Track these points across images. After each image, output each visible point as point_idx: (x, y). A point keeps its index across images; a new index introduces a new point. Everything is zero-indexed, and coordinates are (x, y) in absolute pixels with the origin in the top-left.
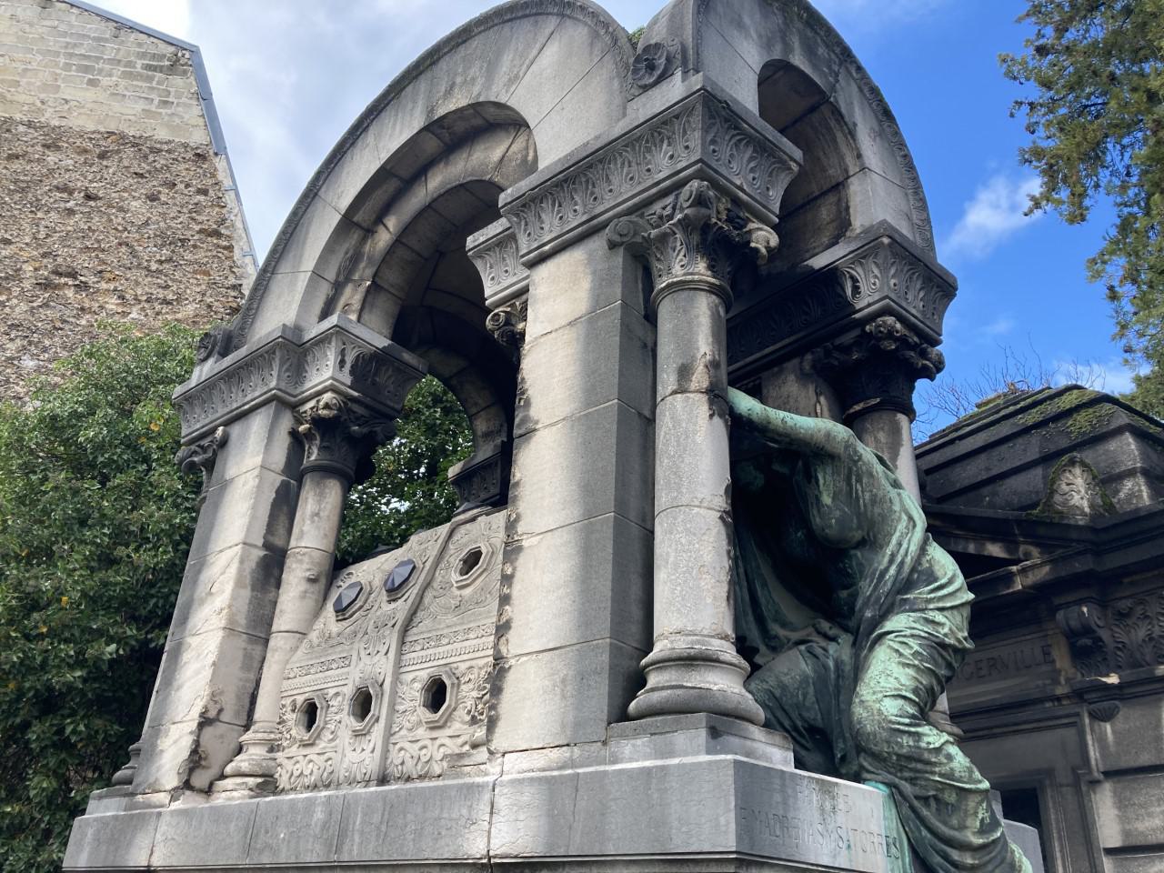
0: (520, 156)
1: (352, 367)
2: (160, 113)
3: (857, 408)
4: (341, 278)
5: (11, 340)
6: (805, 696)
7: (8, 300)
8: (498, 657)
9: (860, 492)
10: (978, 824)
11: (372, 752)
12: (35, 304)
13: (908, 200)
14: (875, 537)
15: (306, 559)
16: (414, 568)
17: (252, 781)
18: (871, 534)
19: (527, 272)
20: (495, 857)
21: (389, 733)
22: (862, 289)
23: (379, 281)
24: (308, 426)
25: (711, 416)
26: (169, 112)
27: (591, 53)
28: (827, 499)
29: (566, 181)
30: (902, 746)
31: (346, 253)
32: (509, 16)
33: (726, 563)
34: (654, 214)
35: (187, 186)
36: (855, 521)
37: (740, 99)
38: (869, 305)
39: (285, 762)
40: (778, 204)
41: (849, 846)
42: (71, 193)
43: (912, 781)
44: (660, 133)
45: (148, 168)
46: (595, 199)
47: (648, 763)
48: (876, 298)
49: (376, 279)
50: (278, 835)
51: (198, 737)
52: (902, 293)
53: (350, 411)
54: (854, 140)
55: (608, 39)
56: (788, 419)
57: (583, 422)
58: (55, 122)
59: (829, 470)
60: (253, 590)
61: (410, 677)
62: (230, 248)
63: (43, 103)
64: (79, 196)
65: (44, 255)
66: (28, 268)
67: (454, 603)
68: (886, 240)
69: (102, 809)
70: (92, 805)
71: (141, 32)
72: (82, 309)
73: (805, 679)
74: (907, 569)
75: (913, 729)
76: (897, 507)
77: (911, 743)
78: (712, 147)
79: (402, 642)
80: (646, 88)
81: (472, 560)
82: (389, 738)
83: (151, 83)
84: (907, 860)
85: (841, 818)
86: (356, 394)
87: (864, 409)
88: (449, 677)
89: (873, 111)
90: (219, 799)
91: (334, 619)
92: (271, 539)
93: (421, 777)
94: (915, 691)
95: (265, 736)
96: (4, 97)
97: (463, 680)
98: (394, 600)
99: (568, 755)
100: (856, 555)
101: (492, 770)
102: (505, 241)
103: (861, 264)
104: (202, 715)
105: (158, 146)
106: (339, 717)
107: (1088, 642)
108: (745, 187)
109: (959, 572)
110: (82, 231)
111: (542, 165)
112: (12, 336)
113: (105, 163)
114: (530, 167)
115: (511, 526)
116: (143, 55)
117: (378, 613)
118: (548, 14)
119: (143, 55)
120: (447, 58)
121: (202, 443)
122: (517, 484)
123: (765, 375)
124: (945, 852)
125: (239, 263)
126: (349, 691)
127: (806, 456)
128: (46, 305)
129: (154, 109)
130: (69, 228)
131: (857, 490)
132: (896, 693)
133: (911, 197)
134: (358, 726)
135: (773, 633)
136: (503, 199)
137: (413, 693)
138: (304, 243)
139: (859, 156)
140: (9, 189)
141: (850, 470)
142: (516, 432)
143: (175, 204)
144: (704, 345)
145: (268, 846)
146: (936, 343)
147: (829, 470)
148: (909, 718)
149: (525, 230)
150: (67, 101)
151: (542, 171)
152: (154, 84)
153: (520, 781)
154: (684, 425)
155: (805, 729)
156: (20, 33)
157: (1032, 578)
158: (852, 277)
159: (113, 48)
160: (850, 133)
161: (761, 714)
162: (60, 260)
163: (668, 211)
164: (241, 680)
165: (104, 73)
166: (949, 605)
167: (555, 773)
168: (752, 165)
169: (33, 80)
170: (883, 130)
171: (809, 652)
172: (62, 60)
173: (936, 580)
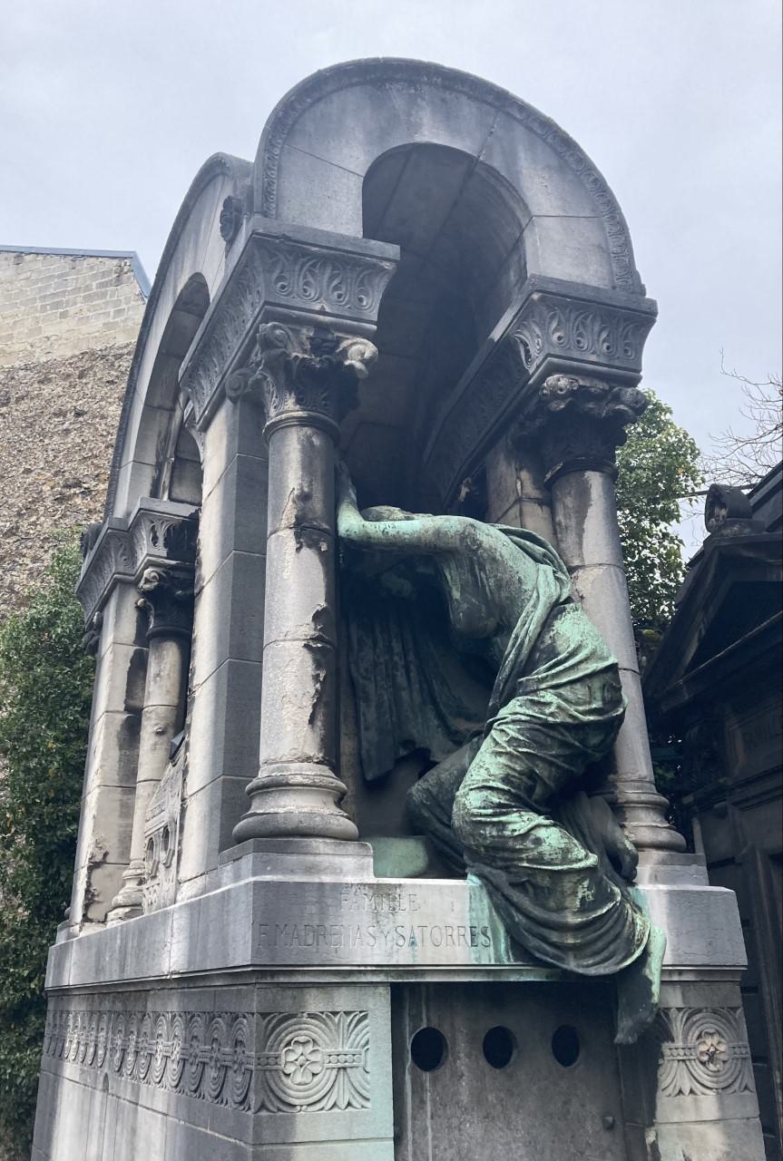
1: (165, 540)
2: (117, 322)
5: (46, 551)
7: (38, 519)
9: (484, 580)
10: (578, 903)
12: (56, 517)
13: (604, 229)
15: (153, 716)
18: (503, 618)
23: (182, 455)
25: (298, 550)
26: (123, 318)
28: (456, 594)
30: (485, 838)
31: (159, 436)
36: (483, 610)
38: (538, 367)
42: (65, 416)
43: (506, 869)
45: (115, 374)
49: (178, 454)
53: (173, 578)
58: (43, 359)
59: (453, 565)
60: (120, 749)
63: (32, 346)
64: (70, 416)
65: (56, 474)
66: (46, 488)
71: (92, 257)
72: (90, 511)
74: (525, 651)
75: (495, 819)
77: (494, 833)
83: (105, 298)
84: (503, 946)
85: (401, 918)
86: (173, 562)
89: (551, 146)
90: (110, 925)
92: (132, 702)
94: (506, 780)
96: (4, 351)
100: (497, 642)
105: (121, 351)
108: (328, 310)
110: (78, 445)
112: (46, 548)
113: (84, 381)
116: (94, 277)
119: (94, 277)
124: (541, 935)
127: (425, 560)
128: (64, 516)
129: (112, 321)
130: (69, 445)
131: (481, 579)
133: (606, 224)
135: (453, 728)
140: (22, 427)
146: (634, 381)
147: (453, 565)
148: (491, 808)
150: (48, 338)
152: (108, 298)
156: (6, 293)
158: (522, 341)
159: (73, 279)
161: (351, 827)
162: (67, 474)
164: (121, 826)
165: (70, 304)
168: (335, 283)
169: (21, 330)
170: (566, 162)
172: (39, 304)
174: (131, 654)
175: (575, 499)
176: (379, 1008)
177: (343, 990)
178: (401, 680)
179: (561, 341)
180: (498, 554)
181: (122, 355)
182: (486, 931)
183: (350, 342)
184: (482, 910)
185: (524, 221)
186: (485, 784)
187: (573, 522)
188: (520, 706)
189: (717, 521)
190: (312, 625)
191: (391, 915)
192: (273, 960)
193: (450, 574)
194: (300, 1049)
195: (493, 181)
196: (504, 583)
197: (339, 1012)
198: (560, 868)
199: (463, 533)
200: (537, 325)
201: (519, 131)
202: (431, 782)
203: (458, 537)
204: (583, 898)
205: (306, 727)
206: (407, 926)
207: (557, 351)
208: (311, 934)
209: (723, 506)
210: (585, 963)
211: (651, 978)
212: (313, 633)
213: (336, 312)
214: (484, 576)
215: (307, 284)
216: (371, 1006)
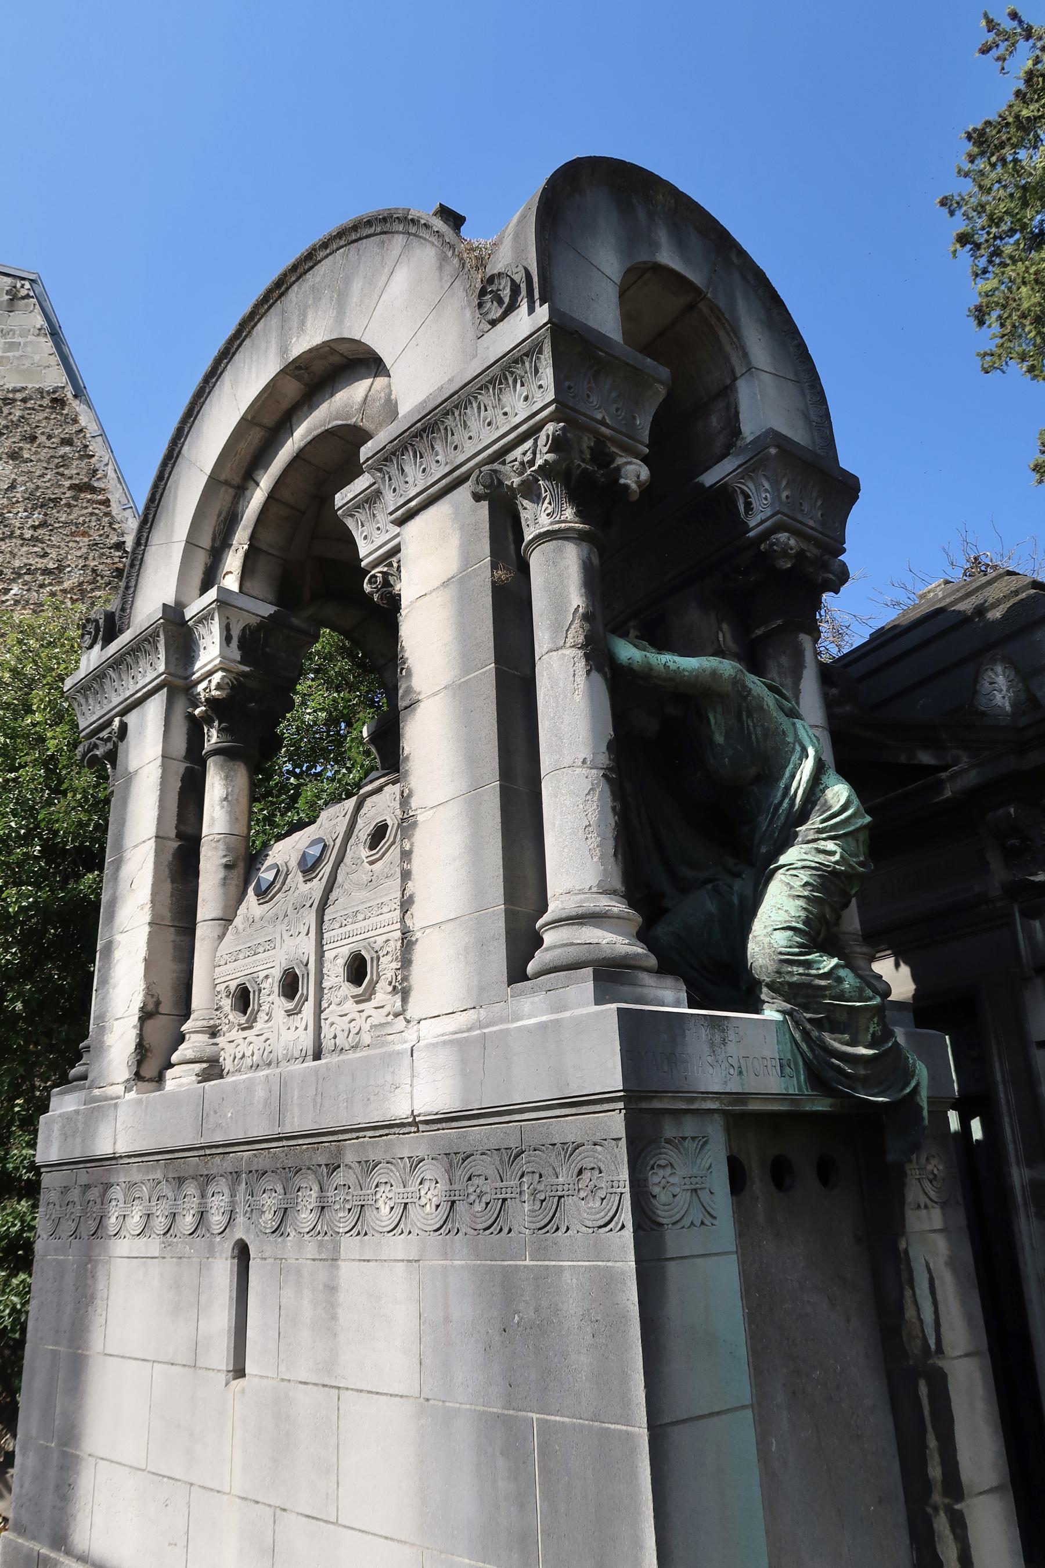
0: (383, 395)
4: (217, 544)
8: (406, 933)
10: (869, 1037)
11: (306, 1029)
16: (325, 846)
17: (198, 1067)
19: (397, 530)
20: (419, 1115)
21: (319, 1011)
22: (754, 505)
24: (203, 708)
25: (588, 672)
26: (17, 354)
27: (441, 279)
28: (719, 739)
29: (424, 430)
31: (219, 516)
32: (354, 237)
34: (516, 460)
35: (49, 437)
37: (592, 323)
38: (762, 522)
39: (227, 1046)
40: (647, 433)
41: (740, 1073)
44: (512, 373)
46: (456, 448)
47: (544, 1018)
48: (769, 514)
50: (226, 1115)
51: (141, 1030)
54: (738, 338)
55: (456, 260)
56: (670, 664)
57: (460, 690)
59: (719, 709)
61: (333, 953)
62: (106, 502)
67: (365, 878)
68: (773, 451)
69: (64, 1104)
70: (52, 1105)
76: (790, 739)
78: (567, 384)
79: (320, 921)
80: (493, 323)
81: (379, 834)
82: (320, 1016)
85: (732, 1048)
86: (247, 669)
87: (764, 633)
88: (368, 951)
90: (170, 1085)
91: (256, 902)
92: (183, 828)
93: (354, 1047)
95: (205, 1023)
97: (381, 953)
98: (309, 880)
99: (476, 1017)
101: (409, 1037)
102: (371, 499)
103: (751, 478)
104: (142, 1009)
105: (11, 396)
106: (271, 1000)
107: (1017, 842)
109: (854, 798)
111: (403, 409)
114: (391, 409)
115: (405, 800)
117: (296, 894)
118: (392, 233)
120: (295, 287)
121: (101, 735)
122: (407, 758)
125: (118, 518)
126: (277, 973)
127: (691, 698)
133: (807, 391)
134: (290, 1006)
136: (366, 451)
137: (335, 971)
138: (174, 509)
139: (746, 355)
142: (402, 704)
143: (39, 460)
145: (218, 1126)
147: (719, 709)
148: (798, 947)
149: (390, 486)
151: (405, 416)
153: (434, 1045)
154: (561, 684)
157: (961, 783)
158: (743, 492)
160: (733, 331)
161: (652, 961)
163: (528, 457)
167: (465, 1035)
168: (614, 395)
173: (830, 808)
174: (182, 771)
176: (716, 1133)
181: (14, 400)
183: (625, 460)
185: (739, 370)
187: (789, 681)
193: (715, 718)
194: (661, 1172)
195: (713, 321)
199: (735, 677)
200: (768, 479)
201: (737, 277)
204: (874, 1032)
205: (612, 859)
206: (735, 1056)
207: (786, 510)
213: (615, 426)
215: (590, 389)
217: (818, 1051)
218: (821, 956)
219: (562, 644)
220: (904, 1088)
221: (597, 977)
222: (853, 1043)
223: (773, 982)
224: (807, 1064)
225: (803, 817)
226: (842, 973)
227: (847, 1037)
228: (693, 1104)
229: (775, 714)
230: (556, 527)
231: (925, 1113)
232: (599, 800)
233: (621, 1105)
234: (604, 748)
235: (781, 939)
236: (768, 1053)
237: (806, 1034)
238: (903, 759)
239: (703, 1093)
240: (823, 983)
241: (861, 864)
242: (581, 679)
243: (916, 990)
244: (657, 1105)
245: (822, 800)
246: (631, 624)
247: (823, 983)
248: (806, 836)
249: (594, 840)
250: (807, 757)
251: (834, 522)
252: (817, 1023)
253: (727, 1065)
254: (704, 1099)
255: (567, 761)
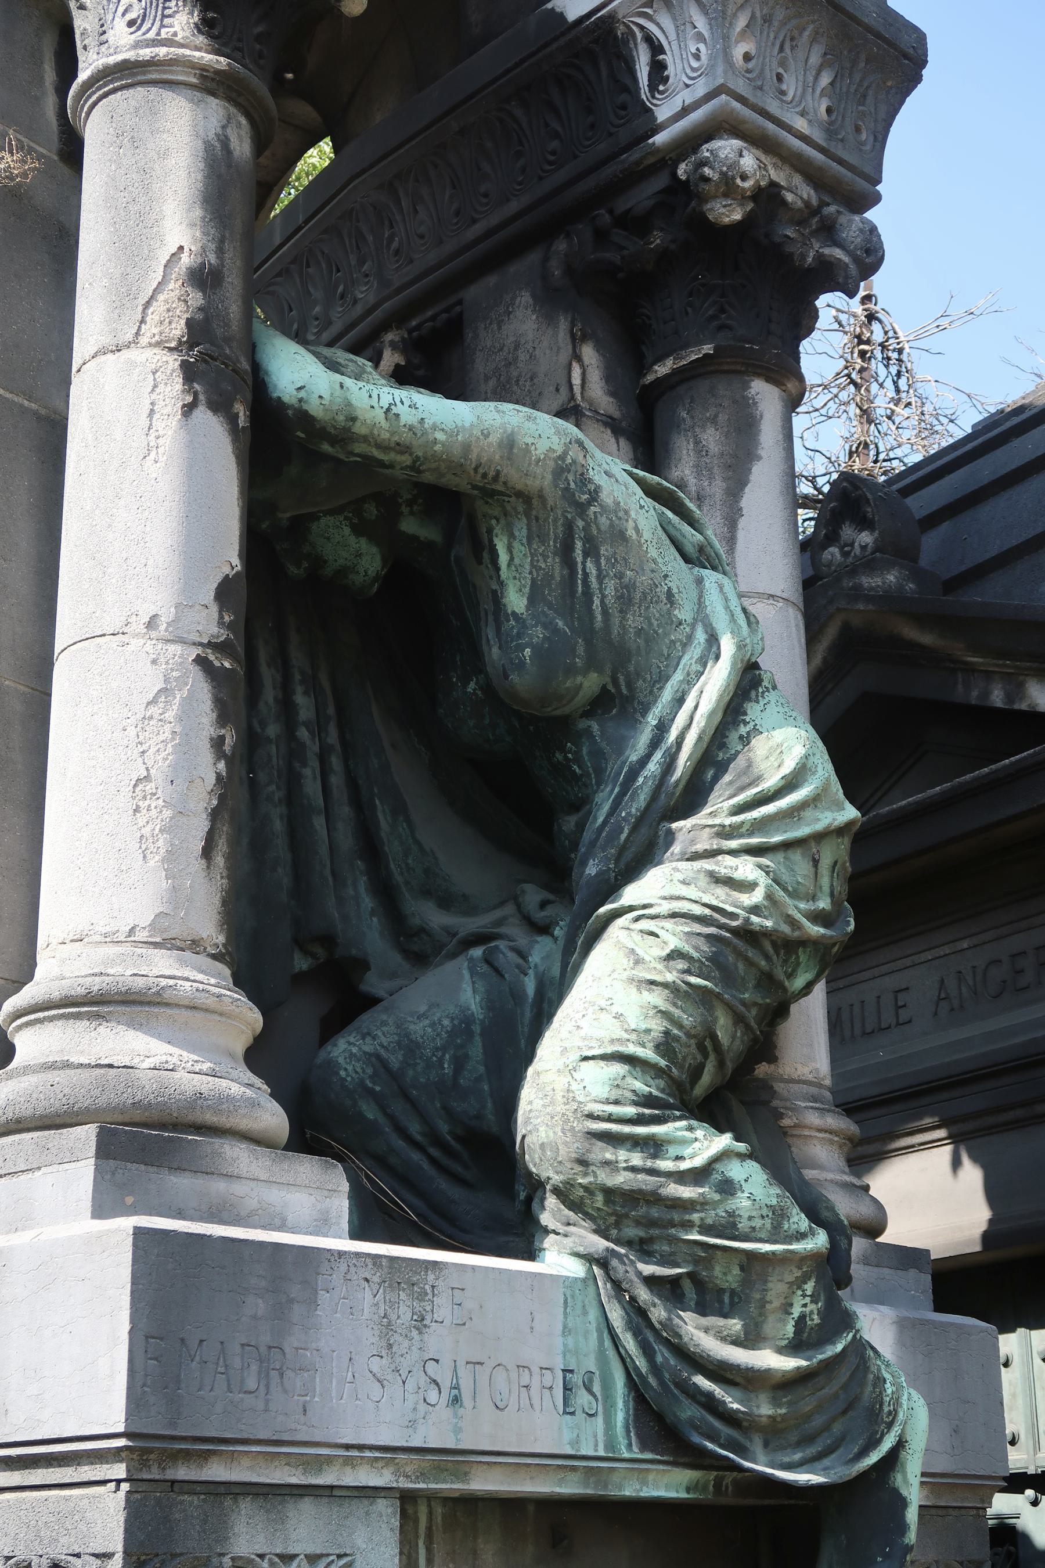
3: (662, 369)
6: (459, 1065)
10: (790, 1329)
14: (630, 685)
22: (670, 71)
25: (188, 409)
28: (516, 601)
33: (208, 770)
36: (581, 650)
38: (685, 111)
41: (456, 1400)
52: (770, 76)
59: (521, 530)
73: (463, 1026)
76: (684, 613)
84: (620, 1417)
87: (675, 372)
100: (588, 732)
123: (472, 293)
131: (586, 575)
132: (609, 1049)
135: (416, 921)
141: (569, 527)
144: (178, 230)
147: (521, 530)
148: (636, 1104)
155: (457, 1138)
158: (649, 39)
161: (273, 1118)
166: (776, 839)
171: (488, 962)
173: (757, 780)
175: (727, 435)
177: (307, 1505)
178: (312, 788)
179: (750, 65)
180: (631, 524)
182: (591, 1380)
184: (586, 1333)
186: (621, 1049)
187: (717, 488)
188: (684, 882)
189: (845, 554)
190: (214, 609)
191: (415, 1333)
192: (173, 1424)
193: (510, 549)
196: (638, 595)
197: (296, 1556)
198: (766, 1248)
199: (562, 457)
200: (704, 9)
202: (385, 1041)
203: (551, 464)
204: (802, 1318)
205: (197, 865)
206: (446, 1361)
207: (740, 86)
208: (254, 1368)
209: (864, 523)
210: (786, 1459)
211: (904, 1492)
212: (215, 630)
214: (590, 566)
216: (360, 1543)
217: (662, 1354)
218: (690, 1129)
219: (129, 336)
220: (864, 1453)
221: (108, 1148)
222: (750, 1340)
223: (569, 1184)
224: (634, 1384)
225: (692, 796)
226: (736, 1170)
227: (735, 1325)
228: (320, 1471)
229: (653, 553)
230: (146, 53)
231: (912, 1515)
232: (180, 719)
233: (119, 1470)
234: (207, 593)
235: (598, 1083)
236: (536, 1358)
237: (637, 1313)
238: (997, 698)
239: (348, 1447)
240: (687, 1192)
241: (818, 917)
242: (169, 423)
243: (991, 1221)
244: (217, 1471)
245: (740, 762)
246: (390, 336)
247: (687, 1192)
248: (693, 842)
249: (157, 814)
250: (717, 657)
251: (858, 130)
252: (668, 1289)
253: (423, 1380)
254: (348, 1461)
255: (111, 621)
